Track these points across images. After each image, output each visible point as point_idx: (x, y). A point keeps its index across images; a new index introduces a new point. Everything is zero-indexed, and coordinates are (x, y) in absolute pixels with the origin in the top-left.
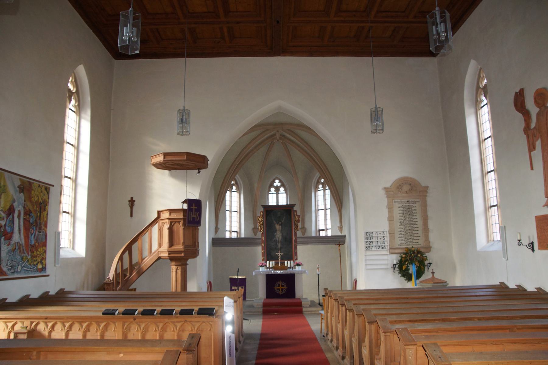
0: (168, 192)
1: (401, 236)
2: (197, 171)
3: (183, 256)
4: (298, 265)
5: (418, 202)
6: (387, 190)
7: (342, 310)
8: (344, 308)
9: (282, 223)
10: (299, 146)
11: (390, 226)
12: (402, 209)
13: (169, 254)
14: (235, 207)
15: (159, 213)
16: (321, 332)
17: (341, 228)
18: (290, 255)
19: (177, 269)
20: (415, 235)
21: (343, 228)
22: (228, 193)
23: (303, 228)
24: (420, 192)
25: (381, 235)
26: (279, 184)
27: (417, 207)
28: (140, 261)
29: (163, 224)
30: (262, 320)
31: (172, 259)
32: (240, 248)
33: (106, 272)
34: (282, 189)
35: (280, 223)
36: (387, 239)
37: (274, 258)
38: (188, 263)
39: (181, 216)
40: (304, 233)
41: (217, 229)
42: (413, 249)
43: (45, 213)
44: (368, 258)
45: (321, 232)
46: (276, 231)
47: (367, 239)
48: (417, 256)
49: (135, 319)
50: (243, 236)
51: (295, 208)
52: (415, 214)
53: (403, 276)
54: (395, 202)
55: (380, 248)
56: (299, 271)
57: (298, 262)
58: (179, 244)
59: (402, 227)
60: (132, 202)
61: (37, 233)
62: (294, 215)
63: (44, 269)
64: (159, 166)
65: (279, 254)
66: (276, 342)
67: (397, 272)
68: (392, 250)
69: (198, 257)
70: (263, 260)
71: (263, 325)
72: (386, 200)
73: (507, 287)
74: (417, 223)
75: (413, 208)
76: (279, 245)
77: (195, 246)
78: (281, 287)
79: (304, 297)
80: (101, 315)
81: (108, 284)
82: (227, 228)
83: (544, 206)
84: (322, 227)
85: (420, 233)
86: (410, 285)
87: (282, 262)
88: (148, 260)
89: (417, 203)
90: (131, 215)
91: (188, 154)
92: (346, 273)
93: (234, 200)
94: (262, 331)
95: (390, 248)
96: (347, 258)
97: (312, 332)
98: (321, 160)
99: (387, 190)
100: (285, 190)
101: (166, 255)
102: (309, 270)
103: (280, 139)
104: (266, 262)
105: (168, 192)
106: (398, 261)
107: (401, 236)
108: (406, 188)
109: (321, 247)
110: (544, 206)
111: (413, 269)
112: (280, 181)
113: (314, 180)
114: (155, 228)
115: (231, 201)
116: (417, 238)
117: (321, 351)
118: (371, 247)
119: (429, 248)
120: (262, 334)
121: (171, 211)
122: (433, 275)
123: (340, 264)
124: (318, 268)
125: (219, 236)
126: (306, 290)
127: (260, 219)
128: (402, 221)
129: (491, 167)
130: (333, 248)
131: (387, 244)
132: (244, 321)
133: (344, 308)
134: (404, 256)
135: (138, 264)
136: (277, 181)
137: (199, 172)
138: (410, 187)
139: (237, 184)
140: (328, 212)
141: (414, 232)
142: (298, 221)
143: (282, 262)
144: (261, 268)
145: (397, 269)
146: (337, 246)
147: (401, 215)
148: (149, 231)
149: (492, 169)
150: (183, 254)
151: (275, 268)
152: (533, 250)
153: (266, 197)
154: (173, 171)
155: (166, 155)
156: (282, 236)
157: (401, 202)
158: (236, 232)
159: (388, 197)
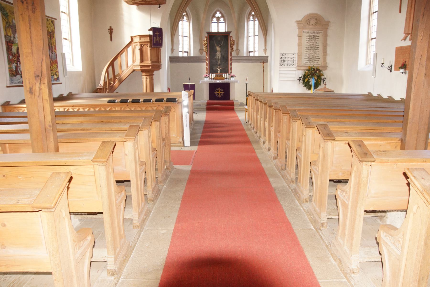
0: (136, 22)
3: (151, 69)
4: (232, 77)
5: (321, 33)
6: (298, 23)
9: (221, 45)
11: (298, 50)
12: (309, 37)
13: (141, 67)
14: (186, 33)
15: (132, 38)
17: (265, 51)
18: (226, 69)
20: (317, 57)
21: (267, 50)
23: (237, 49)
25: (292, 56)
26: (220, 15)
27: (320, 36)
31: (143, 71)
32: (190, 64)
33: (97, 81)
34: (222, 19)
35: (220, 45)
36: (296, 59)
37: (216, 72)
38: (154, 73)
39: (148, 40)
40: (238, 54)
41: (172, 50)
42: (314, 67)
43: (53, 39)
44: (282, 72)
46: (216, 51)
47: (281, 58)
48: (316, 72)
50: (192, 55)
51: (231, 35)
52: (318, 42)
53: (305, 86)
54: (304, 32)
56: (232, 81)
57: (232, 74)
58: (148, 60)
59: (308, 51)
60: (111, 30)
61: (51, 54)
62: (231, 40)
63: (58, 79)
65: (219, 69)
67: (301, 83)
68: (299, 67)
70: (207, 73)
72: (297, 30)
73: (372, 96)
75: (317, 38)
76: (219, 62)
78: (219, 92)
82: (180, 49)
83: (402, 40)
85: (321, 56)
87: (221, 74)
88: (126, 72)
90: (111, 40)
92: (267, 83)
93: (185, 27)
95: (298, 66)
96: (269, 73)
97: (239, 121)
100: (224, 20)
102: (240, 80)
104: (209, 74)
105: (136, 22)
106: (302, 76)
108: (313, 22)
109: (250, 64)
110: (402, 40)
111: (312, 82)
112: (221, 13)
114: (130, 49)
115: (182, 29)
116: (318, 60)
117: (243, 130)
119: (325, 67)
121: (141, 36)
125: (175, 55)
126: (237, 94)
129: (376, 9)
131: (295, 63)
132: (194, 114)
134: (307, 72)
136: (218, 13)
137: (159, 7)
138: (316, 21)
140: (257, 37)
141: (316, 55)
142: (233, 44)
143: (221, 74)
144: (205, 78)
145: (301, 81)
146: (262, 64)
147: (308, 42)
148: (126, 51)
149: (377, 10)
150: (150, 68)
152: (391, 71)
153: (208, 24)
154: (140, 6)
156: (221, 55)
157: (308, 32)
158: (187, 52)
159: (299, 28)
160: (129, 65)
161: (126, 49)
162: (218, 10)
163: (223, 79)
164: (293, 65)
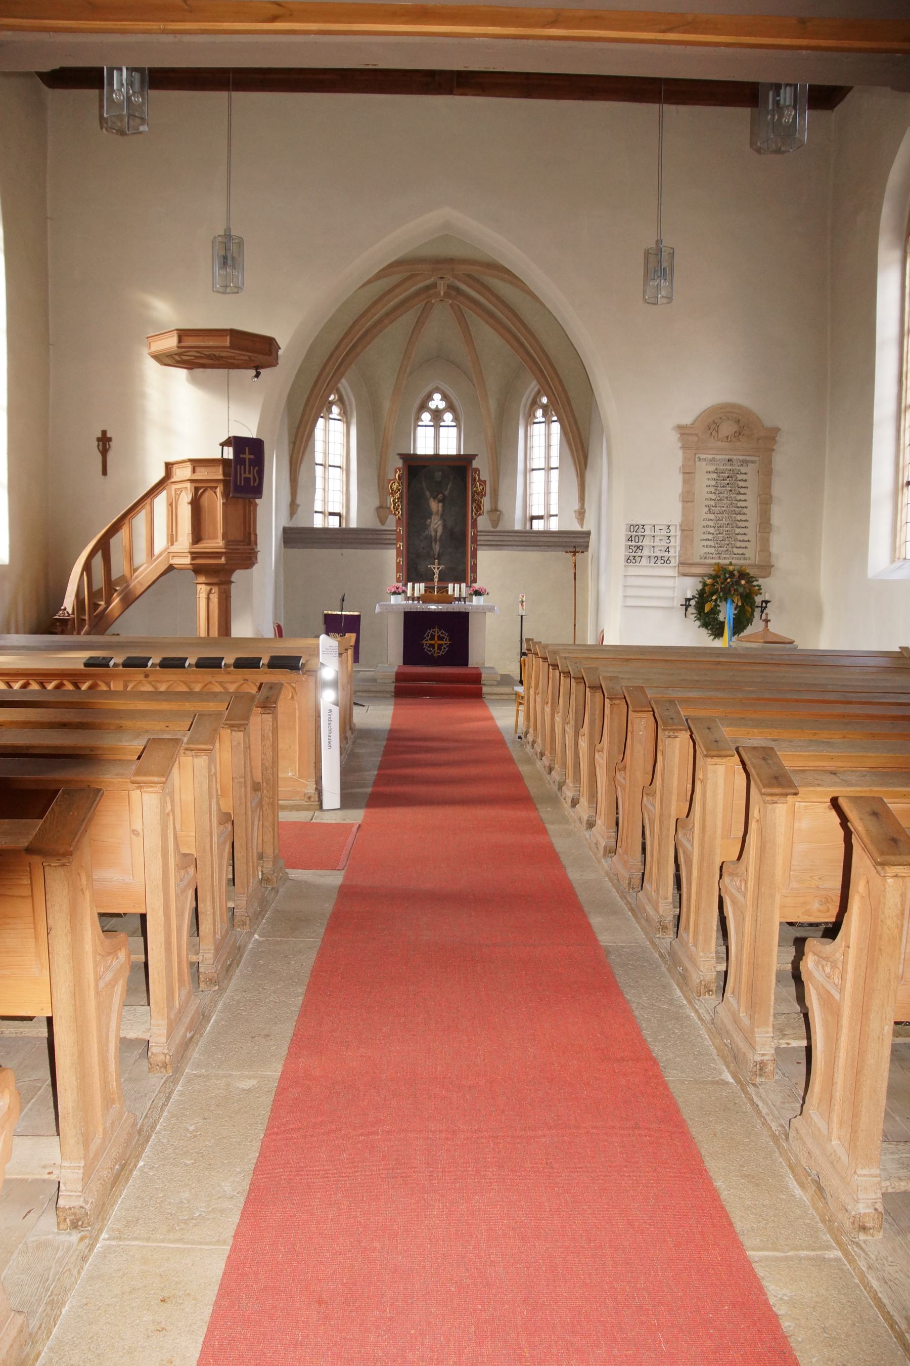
1: (706, 537)
2: (253, 372)
3: (225, 563)
4: (478, 593)
6: (683, 430)
7: (554, 676)
8: (557, 672)
10: (492, 315)
11: (683, 515)
13: (193, 559)
14: (336, 456)
15: (169, 466)
16: (516, 732)
17: (581, 515)
18: (461, 571)
19: (210, 592)
20: (740, 537)
22: (321, 422)
23: (495, 510)
24: (758, 439)
26: (442, 405)
27: (750, 472)
28: (128, 574)
29: (178, 492)
30: (392, 707)
31: (198, 570)
32: (345, 551)
34: (448, 417)
35: (440, 496)
36: (676, 543)
37: (426, 577)
39: (218, 474)
40: (495, 522)
41: (293, 507)
42: (731, 568)
45: (534, 522)
46: (430, 514)
47: (630, 539)
48: (738, 583)
49: (147, 676)
50: (353, 524)
51: (475, 464)
52: (742, 491)
53: (705, 625)
54: (700, 459)
55: (659, 561)
56: (478, 607)
57: (476, 586)
59: (712, 516)
60: (104, 441)
64: (165, 359)
65: (436, 569)
66: (421, 744)
68: (685, 567)
69: (255, 567)
71: (394, 716)
72: (680, 453)
74: (745, 510)
75: (740, 477)
76: (437, 548)
77: (249, 544)
78: (436, 641)
79: (487, 665)
80: (82, 667)
81: (64, 622)
82: (318, 506)
84: (537, 510)
85: (752, 532)
86: (719, 643)
88: (145, 571)
89: (750, 465)
90: (105, 472)
91: (235, 334)
92: (586, 616)
94: (392, 725)
95: (681, 563)
96: (591, 584)
97: (497, 731)
98: (543, 351)
99: (683, 430)
100: (456, 419)
101: (187, 561)
103: (447, 295)
104: (406, 585)
105: (184, 421)
106: (695, 593)
107: (706, 537)
108: (727, 429)
109: (533, 556)
111: (727, 612)
112: (445, 397)
113: (526, 400)
114: (160, 503)
115: (326, 442)
117: (510, 760)
118: (638, 559)
119: (767, 568)
120: (391, 731)
121: (197, 463)
122: (767, 626)
123: (575, 595)
124: (522, 602)
125: (300, 522)
126: (493, 648)
127: (395, 487)
128: (713, 503)
130: (560, 559)
131: (674, 553)
133: (557, 672)
134: (709, 581)
135: (123, 578)
136: (437, 396)
138: (735, 428)
139: (341, 401)
140: (555, 474)
141: (737, 531)
144: (393, 597)
145: (691, 610)
147: (712, 489)
148: (148, 507)
150: (223, 560)
151: (423, 599)
153: (409, 434)
154: (199, 372)
155: (183, 334)
156: (444, 526)
157: (714, 460)
158: (339, 514)
159: (684, 447)
160: (157, 550)
161: (148, 500)
162: (437, 390)
163: (450, 600)
164: (667, 561)
